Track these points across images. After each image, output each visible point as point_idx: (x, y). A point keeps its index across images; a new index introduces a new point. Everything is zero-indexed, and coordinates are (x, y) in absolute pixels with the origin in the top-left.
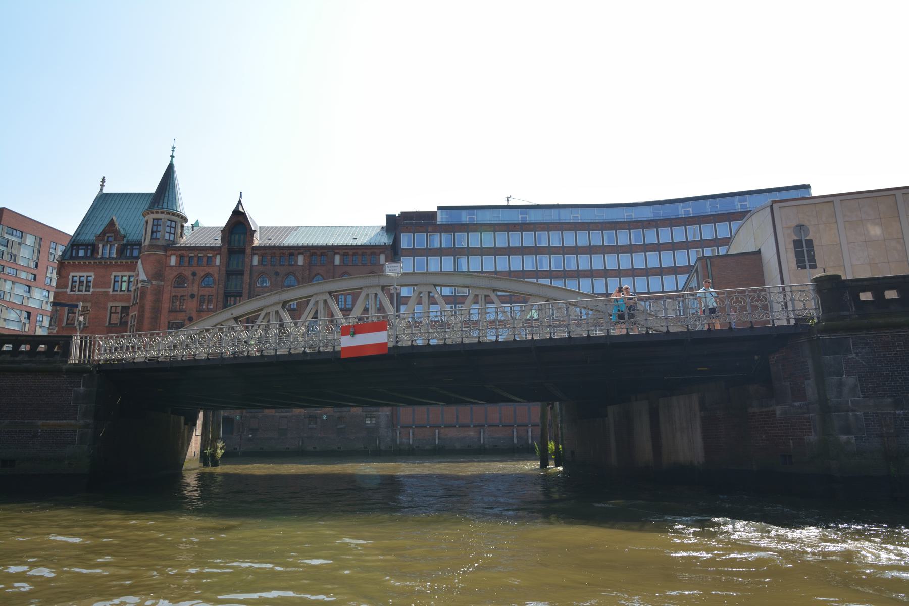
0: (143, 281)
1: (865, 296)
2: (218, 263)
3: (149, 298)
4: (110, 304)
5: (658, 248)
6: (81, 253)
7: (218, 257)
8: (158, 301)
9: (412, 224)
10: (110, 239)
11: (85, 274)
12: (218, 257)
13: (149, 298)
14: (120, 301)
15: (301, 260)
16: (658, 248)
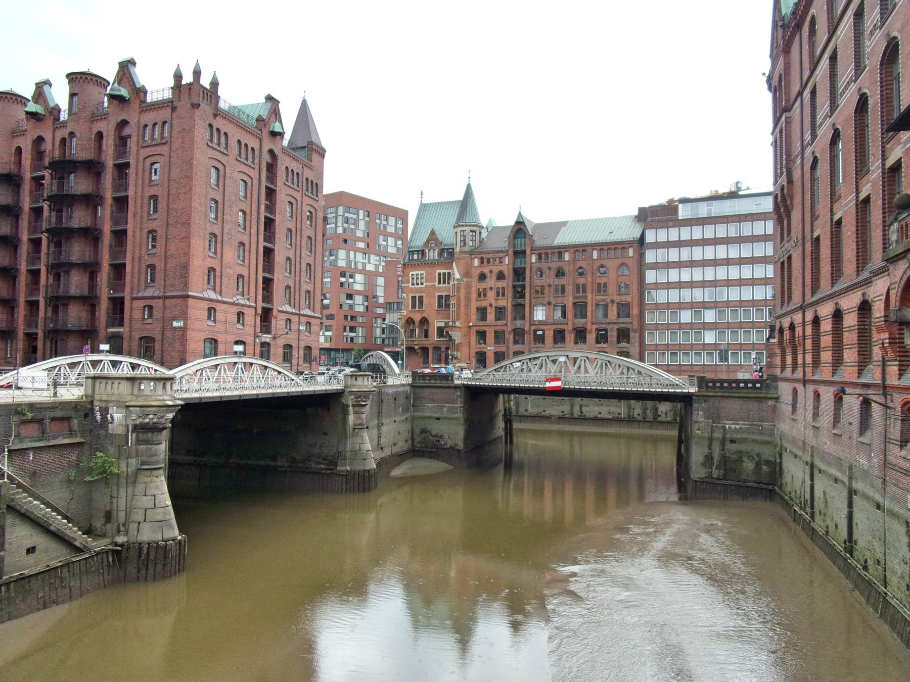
0: (458, 280)
1: (710, 385)
3: (463, 291)
4: (437, 294)
5: (692, 243)
6: (415, 257)
7: (507, 258)
8: (468, 293)
11: (419, 273)
12: (507, 258)
13: (463, 291)
14: (443, 291)
15: (567, 256)
16: (716, 242)
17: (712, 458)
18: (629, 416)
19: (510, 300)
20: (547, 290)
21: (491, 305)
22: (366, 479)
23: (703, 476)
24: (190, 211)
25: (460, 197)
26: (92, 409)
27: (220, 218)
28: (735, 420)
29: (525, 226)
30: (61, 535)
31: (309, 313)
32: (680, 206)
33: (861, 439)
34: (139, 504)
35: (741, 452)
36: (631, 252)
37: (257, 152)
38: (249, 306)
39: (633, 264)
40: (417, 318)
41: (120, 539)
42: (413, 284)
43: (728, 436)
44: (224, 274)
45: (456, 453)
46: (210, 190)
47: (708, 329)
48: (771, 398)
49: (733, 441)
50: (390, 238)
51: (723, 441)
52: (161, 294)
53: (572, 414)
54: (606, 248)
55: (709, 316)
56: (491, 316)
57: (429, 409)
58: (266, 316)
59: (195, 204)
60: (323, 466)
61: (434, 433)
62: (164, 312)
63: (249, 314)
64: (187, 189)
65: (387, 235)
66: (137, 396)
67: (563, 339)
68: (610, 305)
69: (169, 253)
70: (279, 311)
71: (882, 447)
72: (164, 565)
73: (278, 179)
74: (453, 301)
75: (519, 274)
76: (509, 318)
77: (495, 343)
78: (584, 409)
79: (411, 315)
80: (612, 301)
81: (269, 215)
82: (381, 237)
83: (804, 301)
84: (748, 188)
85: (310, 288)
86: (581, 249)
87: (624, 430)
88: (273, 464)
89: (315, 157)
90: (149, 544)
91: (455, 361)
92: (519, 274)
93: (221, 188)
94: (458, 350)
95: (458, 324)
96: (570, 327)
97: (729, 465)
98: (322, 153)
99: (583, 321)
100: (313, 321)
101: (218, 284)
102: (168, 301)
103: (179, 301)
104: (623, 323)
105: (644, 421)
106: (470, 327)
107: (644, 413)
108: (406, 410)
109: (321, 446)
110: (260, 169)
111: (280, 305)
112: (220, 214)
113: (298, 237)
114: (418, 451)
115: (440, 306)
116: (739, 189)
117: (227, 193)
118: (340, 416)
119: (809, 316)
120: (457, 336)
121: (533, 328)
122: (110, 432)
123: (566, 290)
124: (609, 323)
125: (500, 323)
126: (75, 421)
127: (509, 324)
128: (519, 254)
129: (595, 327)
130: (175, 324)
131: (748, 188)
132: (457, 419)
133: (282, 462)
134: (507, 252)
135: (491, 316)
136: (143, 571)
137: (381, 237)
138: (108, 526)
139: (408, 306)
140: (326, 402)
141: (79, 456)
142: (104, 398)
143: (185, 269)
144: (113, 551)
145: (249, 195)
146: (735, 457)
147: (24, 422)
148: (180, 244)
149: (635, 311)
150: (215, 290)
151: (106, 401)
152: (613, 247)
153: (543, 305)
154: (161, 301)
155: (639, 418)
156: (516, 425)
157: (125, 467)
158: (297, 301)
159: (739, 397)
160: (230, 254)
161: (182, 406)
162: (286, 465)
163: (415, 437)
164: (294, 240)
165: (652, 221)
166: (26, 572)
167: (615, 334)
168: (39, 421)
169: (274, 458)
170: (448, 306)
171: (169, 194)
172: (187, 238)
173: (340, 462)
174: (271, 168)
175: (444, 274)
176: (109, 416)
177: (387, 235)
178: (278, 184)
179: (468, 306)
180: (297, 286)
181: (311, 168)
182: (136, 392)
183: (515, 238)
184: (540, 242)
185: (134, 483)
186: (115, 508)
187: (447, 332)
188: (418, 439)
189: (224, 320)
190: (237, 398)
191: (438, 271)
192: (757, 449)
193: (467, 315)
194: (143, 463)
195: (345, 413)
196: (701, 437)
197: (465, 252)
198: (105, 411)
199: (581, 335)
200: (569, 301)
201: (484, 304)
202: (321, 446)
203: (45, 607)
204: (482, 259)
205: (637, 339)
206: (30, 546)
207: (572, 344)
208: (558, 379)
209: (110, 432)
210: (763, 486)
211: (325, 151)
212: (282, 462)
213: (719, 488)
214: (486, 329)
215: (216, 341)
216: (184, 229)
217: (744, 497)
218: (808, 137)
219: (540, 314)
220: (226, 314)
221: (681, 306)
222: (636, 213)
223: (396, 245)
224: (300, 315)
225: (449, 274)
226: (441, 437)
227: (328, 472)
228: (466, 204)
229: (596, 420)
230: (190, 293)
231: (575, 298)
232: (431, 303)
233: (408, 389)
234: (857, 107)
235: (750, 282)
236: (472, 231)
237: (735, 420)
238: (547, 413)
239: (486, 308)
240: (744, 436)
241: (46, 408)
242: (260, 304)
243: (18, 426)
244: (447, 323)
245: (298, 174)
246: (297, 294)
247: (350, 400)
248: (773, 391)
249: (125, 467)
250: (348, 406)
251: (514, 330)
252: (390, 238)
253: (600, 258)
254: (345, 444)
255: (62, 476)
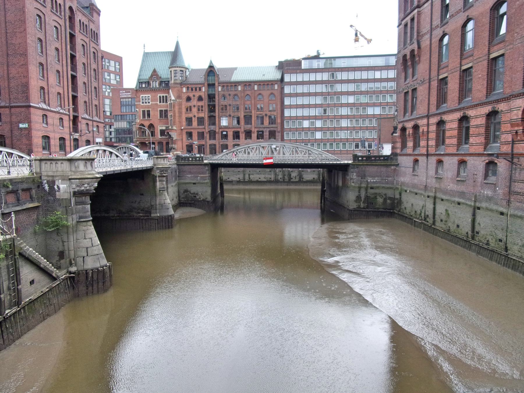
0: (173, 100)
1: (360, 159)
2: (204, 90)
3: (177, 107)
4: (159, 109)
6: (144, 86)
8: (180, 109)
9: (289, 69)
10: (155, 79)
11: (147, 95)
13: (177, 107)
15: (240, 88)
17: (361, 197)
18: (276, 180)
19: (206, 113)
20: (228, 107)
21: (195, 116)
22: (170, 221)
23: (355, 207)
24: (26, 45)
25: (173, 50)
26: (41, 183)
27: (43, 51)
28: (373, 177)
29: (214, 68)
30: (46, 270)
31: (98, 120)
32: (303, 61)
33: (485, 181)
34: (81, 245)
35: (376, 194)
36: (276, 87)
37: (62, 7)
38: (66, 114)
39: (278, 94)
40: (147, 124)
41: (73, 269)
42: (143, 103)
43: (369, 185)
44: (50, 92)
45: (206, 203)
46: (37, 32)
47: (317, 131)
48: (393, 165)
49: (372, 188)
50: (111, 75)
51: (366, 189)
52: (7, 105)
53: (244, 179)
54: (262, 84)
55: (319, 124)
56: (195, 123)
57: (188, 178)
58: (75, 120)
59: (29, 41)
60: (141, 215)
61: (192, 192)
62: (11, 117)
63: (66, 118)
64: (22, 29)
65: (110, 73)
66: (75, 172)
67: (250, 137)
68: (265, 117)
69: (11, 76)
70: (82, 118)
71: (508, 184)
72: (104, 283)
73: (76, 28)
74: (170, 114)
75: (211, 97)
76: (206, 125)
77: (198, 139)
78: (251, 176)
79: (143, 122)
80: (266, 115)
81: (72, 53)
82: (106, 74)
83: (429, 112)
84: (324, 54)
85: (97, 103)
86: (248, 84)
87: (242, 187)
88: (106, 215)
89: (95, 14)
90: (92, 270)
91: (174, 150)
92: (211, 97)
93: (43, 30)
94: (175, 144)
95: (174, 128)
96: (242, 130)
97: (370, 201)
98: (98, 13)
99: (249, 126)
100: (100, 125)
101: (47, 99)
102: (13, 110)
103: (23, 109)
104: (272, 127)
105: (284, 182)
106: (182, 130)
107: (284, 177)
108: (176, 179)
109: (139, 203)
110: (65, 20)
111: (82, 114)
112: (44, 50)
113: (89, 69)
114: (183, 203)
115: (161, 116)
116: (319, 54)
117: (47, 34)
118: (151, 184)
119: (434, 120)
120: (174, 135)
121: (221, 130)
122: (57, 197)
123: (240, 108)
124: (264, 128)
125: (200, 127)
126: (34, 191)
127: (207, 128)
128: (211, 86)
129: (256, 130)
130: (21, 126)
131: (324, 54)
132: (207, 183)
133: (113, 214)
134: (204, 84)
135: (195, 123)
136: (90, 288)
137: (106, 74)
138: (62, 261)
139: (140, 117)
140: (142, 175)
141: (37, 216)
142: (50, 174)
143: (26, 87)
144: (70, 277)
145: (60, 37)
146: (372, 196)
147: (8, 193)
148: (20, 70)
149: (279, 121)
150: (45, 102)
151: (53, 176)
152: (266, 84)
153: (227, 116)
154: (7, 109)
155: (281, 180)
156: (225, 187)
157: (71, 221)
158: (91, 111)
159: (376, 165)
160: (53, 78)
161: (101, 178)
162: (116, 215)
163: (181, 194)
164: (86, 71)
165: (287, 69)
166: (32, 297)
167: (268, 134)
168: (14, 192)
169: (107, 211)
170: (166, 116)
171: (7, 33)
172: (25, 65)
173: (152, 211)
174: (71, 19)
175: (163, 97)
176: (56, 187)
177: (110, 73)
178: (76, 32)
179: (180, 116)
180: (90, 102)
181: (93, 22)
182: (73, 169)
183: (208, 76)
184: (222, 79)
185: (76, 231)
186: (66, 248)
187: (168, 133)
188: (182, 196)
189: (52, 123)
190: (113, 173)
191: (159, 95)
192: (384, 191)
193: (180, 122)
194: (81, 217)
195: (155, 182)
196: (354, 187)
197: (177, 83)
198: (52, 183)
199: (248, 134)
200: (242, 115)
201: (190, 115)
202: (139, 203)
203: (44, 319)
204: (188, 88)
205: (280, 137)
206: (31, 279)
207: (244, 140)
208: (271, 158)
209: (57, 197)
210: (388, 211)
211: (100, 11)
212: (113, 214)
213: (364, 213)
214: (192, 130)
215: (48, 137)
216: (22, 59)
217: (377, 217)
218: (437, 21)
219: (224, 122)
220: (54, 119)
221: (304, 118)
222: (277, 64)
223: (116, 79)
224: (93, 121)
225: (166, 97)
226: (197, 194)
227: (145, 218)
228: (175, 55)
229: (258, 182)
230: (31, 104)
231: (245, 112)
232: (155, 116)
233: (175, 166)
234: (494, 5)
235: (295, 106)
236: (181, 71)
237: (374, 177)
238: (230, 179)
239: (191, 118)
240: (378, 185)
241: (19, 182)
242: (72, 113)
243: (5, 195)
244: (166, 127)
245: (86, 25)
246: (91, 107)
247: (157, 173)
248: (394, 161)
249: (71, 221)
250: (156, 177)
251: (209, 132)
252: (111, 75)
253: (259, 90)
254: (156, 201)
255: (31, 230)
